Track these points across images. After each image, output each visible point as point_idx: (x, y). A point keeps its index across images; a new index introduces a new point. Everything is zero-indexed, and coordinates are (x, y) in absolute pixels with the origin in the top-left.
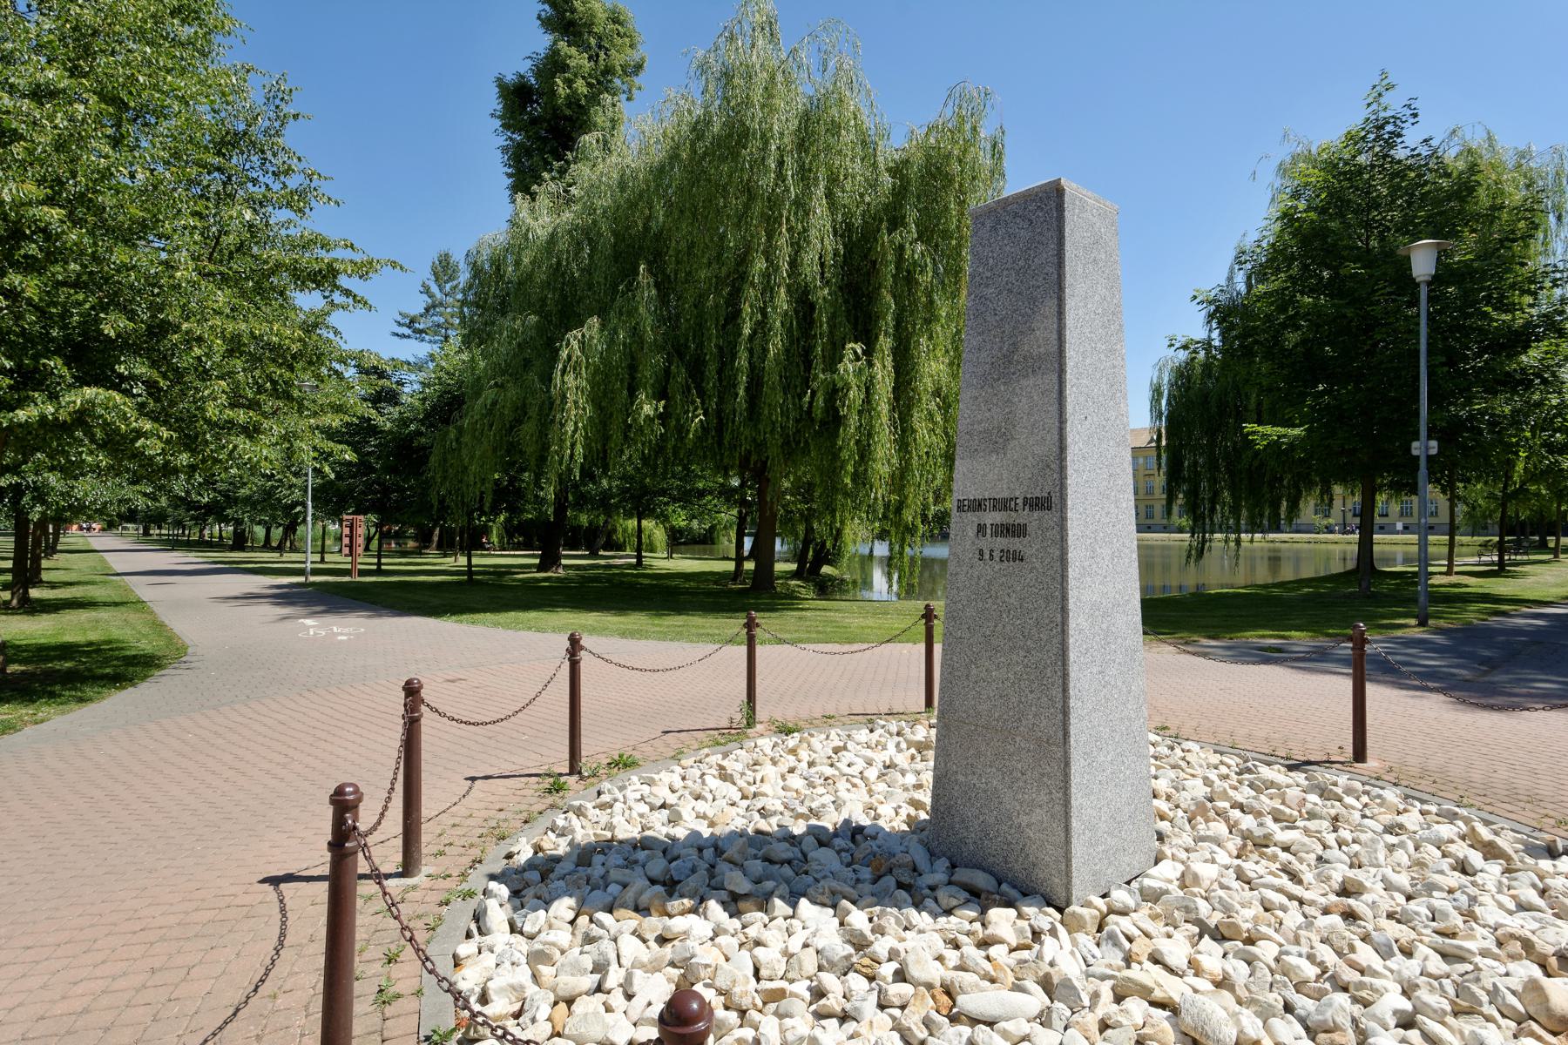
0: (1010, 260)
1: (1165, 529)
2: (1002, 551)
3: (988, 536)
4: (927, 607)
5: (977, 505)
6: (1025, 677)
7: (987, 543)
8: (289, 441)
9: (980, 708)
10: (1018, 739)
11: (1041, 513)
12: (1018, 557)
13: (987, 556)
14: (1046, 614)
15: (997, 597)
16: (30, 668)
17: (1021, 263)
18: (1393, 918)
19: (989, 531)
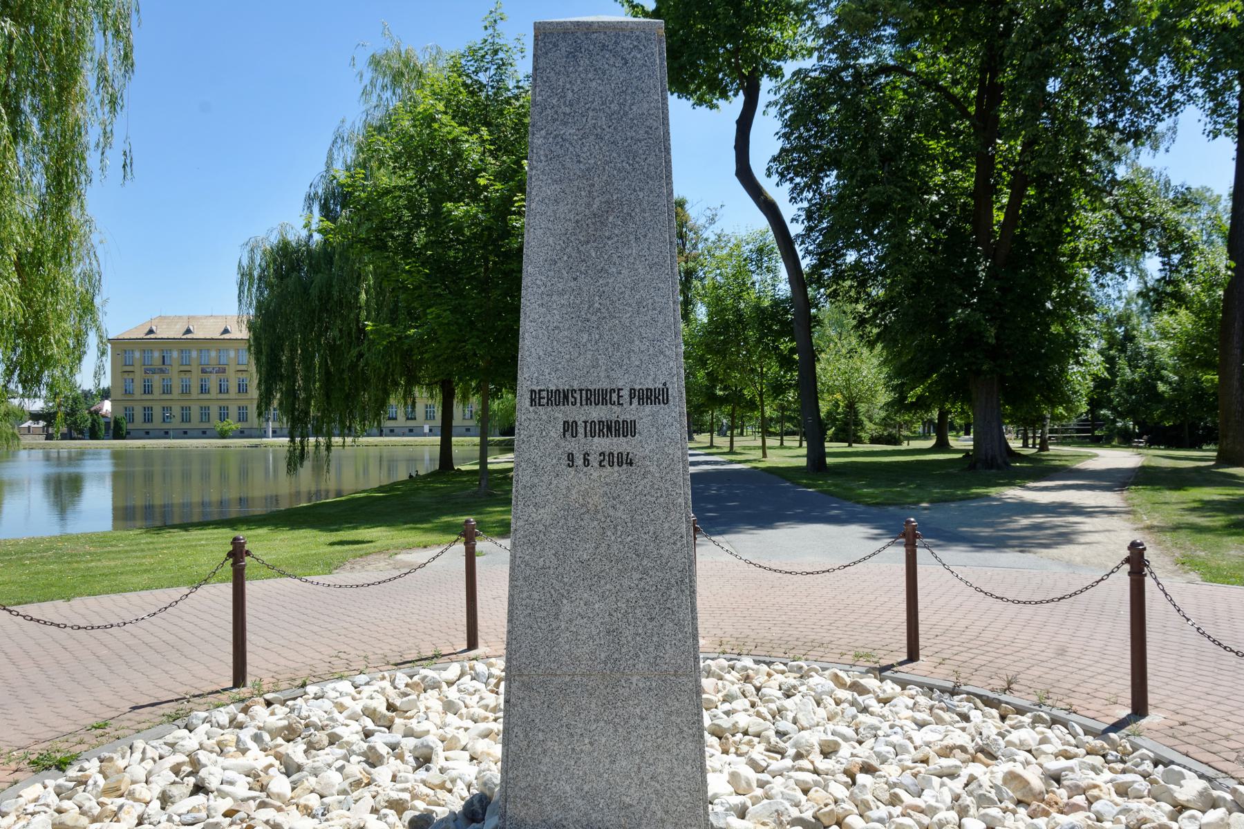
0: (598, 101)
1: (204, 434)
2: (602, 454)
4: (235, 541)
5: (562, 397)
6: (641, 603)
7: (575, 445)
9: (578, 652)
10: (634, 680)
11: (655, 408)
12: (625, 460)
13: (579, 461)
14: (666, 525)
15: (597, 511)
17: (614, 107)
19: (581, 430)
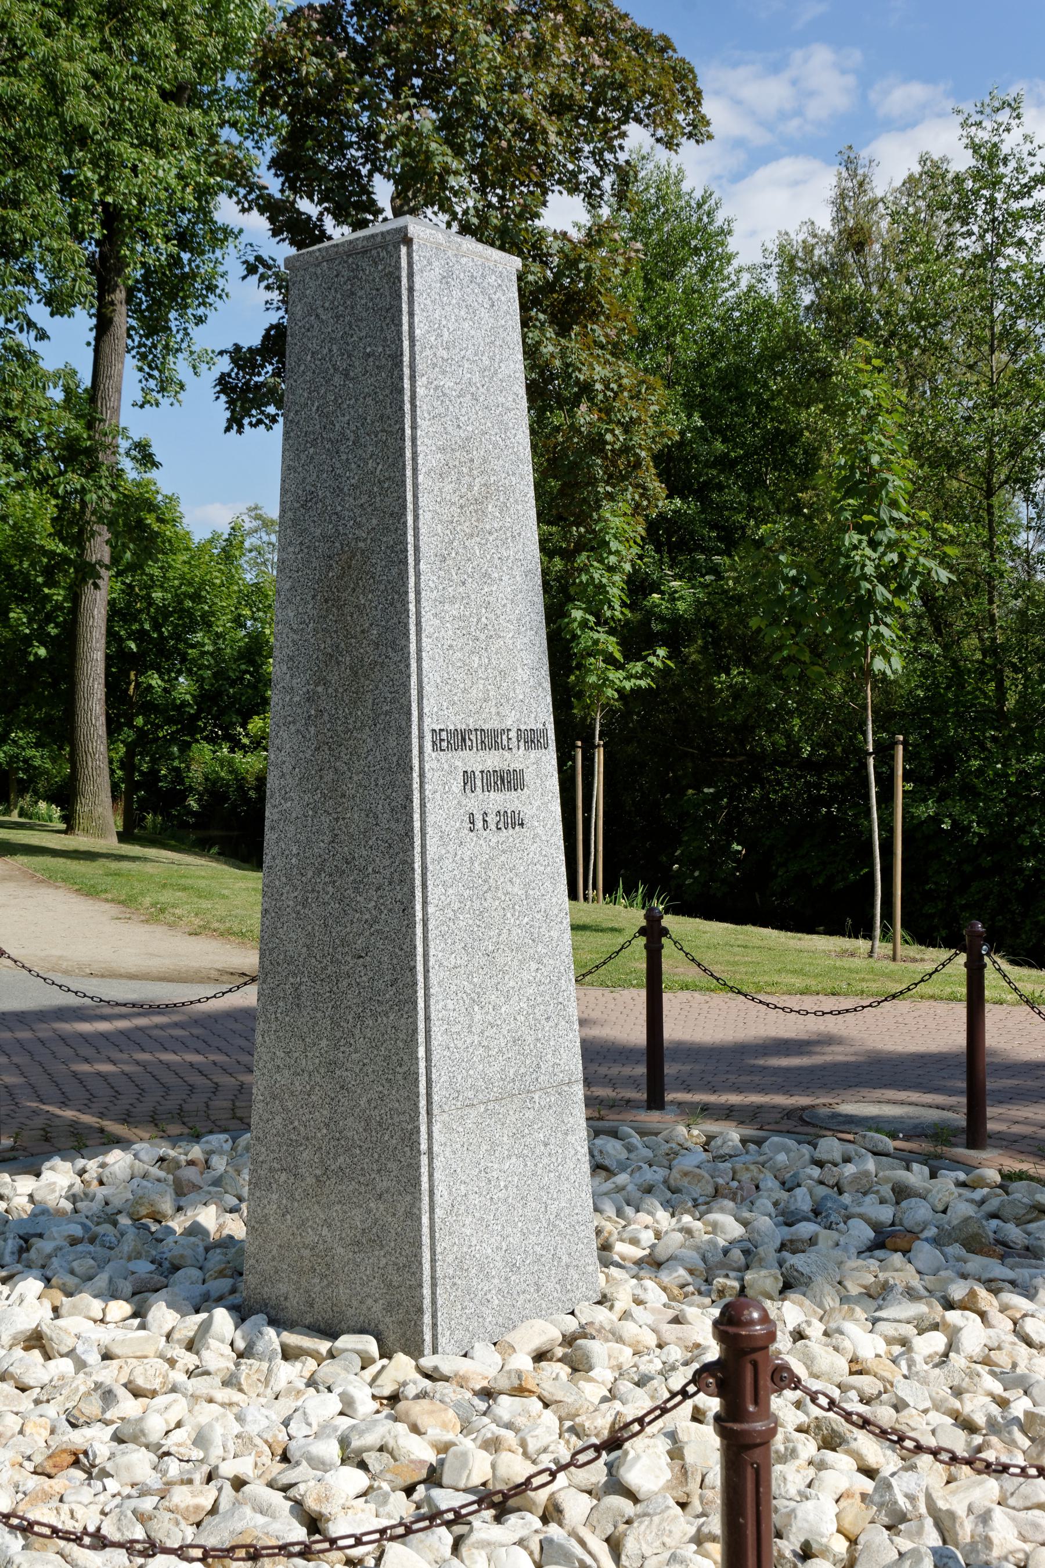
3: (479, 790)
5: (460, 740)
6: (539, 1000)
8: (983, 158)
12: (513, 821)
13: (479, 824)
14: (554, 900)
16: (761, 1062)
18: (41, 1402)
19: (479, 783)
